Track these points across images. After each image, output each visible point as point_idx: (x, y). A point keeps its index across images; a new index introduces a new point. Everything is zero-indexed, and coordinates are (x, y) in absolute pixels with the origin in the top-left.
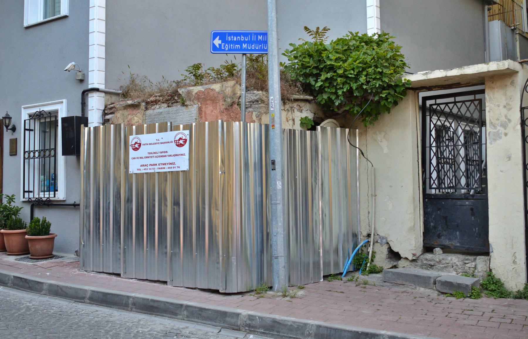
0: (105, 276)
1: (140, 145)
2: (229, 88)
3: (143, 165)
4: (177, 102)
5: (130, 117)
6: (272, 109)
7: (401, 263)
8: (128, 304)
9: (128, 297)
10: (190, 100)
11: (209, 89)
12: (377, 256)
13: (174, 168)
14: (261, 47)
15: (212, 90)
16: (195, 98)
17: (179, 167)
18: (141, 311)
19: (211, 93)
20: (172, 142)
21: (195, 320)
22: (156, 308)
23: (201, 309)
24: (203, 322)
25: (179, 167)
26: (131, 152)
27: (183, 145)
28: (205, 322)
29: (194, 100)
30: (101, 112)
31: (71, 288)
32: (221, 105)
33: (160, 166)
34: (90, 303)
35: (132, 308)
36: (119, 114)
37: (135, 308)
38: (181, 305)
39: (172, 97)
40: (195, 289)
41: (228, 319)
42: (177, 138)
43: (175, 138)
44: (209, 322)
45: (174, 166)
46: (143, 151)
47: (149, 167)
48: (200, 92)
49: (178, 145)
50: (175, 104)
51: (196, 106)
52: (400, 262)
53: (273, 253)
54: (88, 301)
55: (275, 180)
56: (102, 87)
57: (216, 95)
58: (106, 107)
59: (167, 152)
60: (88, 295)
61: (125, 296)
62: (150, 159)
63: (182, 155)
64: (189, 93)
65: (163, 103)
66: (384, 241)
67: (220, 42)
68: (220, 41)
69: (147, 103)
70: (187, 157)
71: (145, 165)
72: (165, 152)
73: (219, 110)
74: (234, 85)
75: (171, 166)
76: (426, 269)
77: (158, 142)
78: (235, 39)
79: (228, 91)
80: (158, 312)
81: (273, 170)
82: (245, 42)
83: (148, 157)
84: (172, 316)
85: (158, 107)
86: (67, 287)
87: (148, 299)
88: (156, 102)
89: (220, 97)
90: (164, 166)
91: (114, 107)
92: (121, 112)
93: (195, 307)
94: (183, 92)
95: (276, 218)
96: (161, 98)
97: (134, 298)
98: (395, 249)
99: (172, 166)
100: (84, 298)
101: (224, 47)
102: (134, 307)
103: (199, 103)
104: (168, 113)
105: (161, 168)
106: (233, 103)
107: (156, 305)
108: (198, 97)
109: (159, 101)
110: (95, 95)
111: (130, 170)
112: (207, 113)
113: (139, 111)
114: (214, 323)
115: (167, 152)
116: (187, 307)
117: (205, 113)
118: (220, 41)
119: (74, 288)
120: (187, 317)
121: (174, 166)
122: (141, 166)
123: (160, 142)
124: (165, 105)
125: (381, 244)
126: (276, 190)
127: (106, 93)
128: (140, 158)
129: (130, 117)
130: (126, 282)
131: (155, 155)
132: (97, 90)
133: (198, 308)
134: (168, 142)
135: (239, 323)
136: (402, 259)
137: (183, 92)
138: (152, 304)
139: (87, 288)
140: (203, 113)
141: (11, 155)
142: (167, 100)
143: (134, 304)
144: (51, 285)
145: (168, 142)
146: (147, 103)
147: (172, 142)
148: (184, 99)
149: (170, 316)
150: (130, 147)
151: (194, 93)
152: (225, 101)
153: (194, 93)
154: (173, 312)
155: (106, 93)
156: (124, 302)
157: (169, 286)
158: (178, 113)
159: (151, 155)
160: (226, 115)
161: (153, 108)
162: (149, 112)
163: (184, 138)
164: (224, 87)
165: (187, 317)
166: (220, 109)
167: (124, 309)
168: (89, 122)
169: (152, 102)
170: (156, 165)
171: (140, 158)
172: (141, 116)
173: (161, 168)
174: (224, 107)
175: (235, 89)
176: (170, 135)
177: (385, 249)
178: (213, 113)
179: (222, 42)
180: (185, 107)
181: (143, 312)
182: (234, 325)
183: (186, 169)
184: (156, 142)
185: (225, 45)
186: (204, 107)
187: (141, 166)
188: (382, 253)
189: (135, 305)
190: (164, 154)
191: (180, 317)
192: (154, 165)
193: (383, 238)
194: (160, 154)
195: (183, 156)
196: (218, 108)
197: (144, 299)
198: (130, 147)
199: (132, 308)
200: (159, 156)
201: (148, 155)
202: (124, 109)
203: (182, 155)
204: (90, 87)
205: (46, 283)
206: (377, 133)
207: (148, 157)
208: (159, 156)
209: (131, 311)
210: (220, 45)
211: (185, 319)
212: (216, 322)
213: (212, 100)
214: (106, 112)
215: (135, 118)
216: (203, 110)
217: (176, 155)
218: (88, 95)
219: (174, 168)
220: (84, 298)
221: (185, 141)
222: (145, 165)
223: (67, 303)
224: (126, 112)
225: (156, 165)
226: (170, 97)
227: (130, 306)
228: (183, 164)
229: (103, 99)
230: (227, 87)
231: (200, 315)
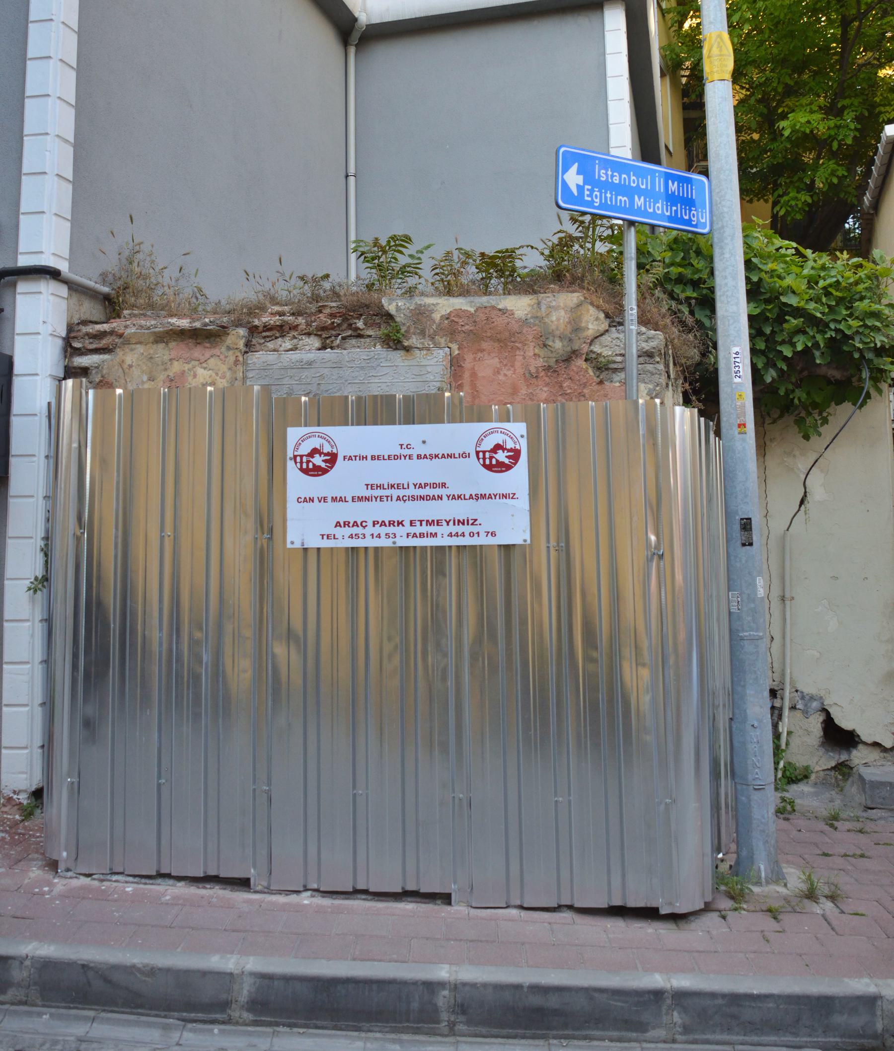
0: (181, 889)
1: (332, 459)
2: (562, 313)
3: (347, 524)
4: (360, 336)
5: (176, 367)
6: (737, 380)
7: (858, 756)
8: (436, 1010)
9: (431, 987)
10: (423, 333)
11: (493, 307)
12: (795, 742)
13: (472, 534)
14: (676, 211)
15: (503, 311)
16: (440, 328)
17: (493, 534)
18: (495, 1031)
19: (500, 321)
20: (465, 455)
21: (719, 1037)
22: (556, 1012)
23: (736, 999)
24: (747, 1038)
25: (493, 534)
26: (295, 478)
27: (508, 468)
28: (755, 1039)
29: (435, 333)
30: (59, 343)
31: (153, 972)
32: (532, 357)
33: (418, 529)
34: (256, 1023)
35: (452, 1025)
36: (130, 357)
37: (469, 1023)
38: (657, 994)
39: (345, 320)
40: (558, 909)
41: (839, 1019)
42: (487, 445)
43: (479, 443)
44: (773, 1038)
45: (474, 529)
46: (344, 479)
47: (370, 530)
48: (459, 313)
49: (489, 467)
50: (353, 341)
51: (441, 354)
52: (855, 752)
53: (750, 777)
54: (247, 1016)
55: (749, 573)
56: (63, 267)
57: (515, 327)
58: (70, 328)
59: (444, 485)
60: (245, 991)
61: (415, 983)
62: (373, 504)
63: (504, 496)
64: (421, 314)
65: (309, 334)
66: (815, 705)
67: (580, 180)
68: (581, 177)
69: (253, 330)
70: (523, 503)
71: (355, 524)
72: (434, 486)
73: (520, 371)
74: (579, 305)
75: (460, 529)
76: (78, 671)
77: (406, 452)
78: (616, 180)
79: (558, 319)
80: (565, 1026)
81: (744, 545)
82: (639, 191)
83: (367, 499)
84: (624, 1034)
85: (287, 344)
86: (130, 970)
87: (518, 987)
88: (282, 330)
89: (529, 333)
90: (433, 529)
91: (112, 333)
92: (140, 349)
93: (713, 995)
94: (398, 309)
95: (756, 679)
96: (301, 320)
97: (456, 987)
98: (845, 722)
99: (467, 529)
100: (224, 1006)
101: (590, 195)
102: (462, 1018)
103: (455, 346)
104: (337, 365)
105: (422, 535)
106: (569, 358)
107: (553, 1002)
108: (451, 327)
109: (295, 327)
110: (47, 289)
111: (289, 539)
112: (480, 375)
113: (216, 351)
114: (789, 1039)
115: (444, 485)
116: (681, 997)
117: (474, 375)
118: (581, 177)
119: (168, 971)
120: (686, 1030)
121: (474, 529)
122: (338, 524)
123: (415, 453)
124: (316, 342)
125: (806, 713)
126: (754, 601)
127: (74, 287)
128: (334, 499)
129: (176, 367)
130: (284, 908)
131: (395, 493)
132: (53, 274)
133: (724, 996)
134: (450, 456)
135: (879, 1026)
136: (860, 746)
137: (398, 309)
138: (536, 1000)
139: (229, 963)
140: (467, 375)
141: (750, 519)
142: (324, 329)
143: (461, 1009)
144: (47, 965)
145: (450, 456)
146: (253, 330)
147: (465, 455)
148: (403, 329)
149: (615, 1034)
150: (290, 464)
151: (437, 316)
152: (545, 345)
153: (437, 316)
154: (626, 1022)
155: (74, 287)
156: (415, 1005)
157: (458, 909)
158: (373, 368)
159: (376, 492)
160: (547, 385)
161: (271, 345)
162: (259, 358)
163: (510, 445)
164: (543, 307)
165: (686, 1030)
166: (527, 367)
167: (417, 1031)
168: (18, 368)
169: (267, 328)
170: (400, 523)
171: (334, 499)
172: (224, 368)
173: (422, 535)
174: (540, 362)
175: (580, 318)
176: (464, 435)
177: (815, 724)
178: (501, 377)
179: (585, 183)
180: (402, 353)
181: (504, 1032)
182: (863, 1036)
183: (519, 541)
184: (398, 451)
185: (592, 191)
186: (469, 357)
187: (338, 524)
188: (808, 733)
189: (464, 1012)
190: (431, 491)
191: (661, 1033)
192: (392, 523)
193: (812, 698)
194: (412, 491)
195: (508, 501)
196: (518, 364)
197: (499, 988)
198: (290, 464)
199: (452, 1025)
200: (413, 498)
201: (368, 493)
202: (156, 342)
203: (504, 496)
204: (23, 261)
205: (21, 960)
206: (797, 453)
207: (367, 499)
208: (413, 498)
209: (452, 1031)
210: (580, 188)
211: (678, 1037)
212: (796, 1035)
213: (499, 341)
214: (76, 345)
215: (200, 371)
216: (468, 364)
217: (483, 497)
218: (14, 285)
219: (472, 534)
220: (224, 1006)
221: (515, 455)
222: (355, 524)
223: (155, 1034)
224: (161, 352)
225: (400, 523)
226: (337, 321)
227: (444, 1016)
228: (509, 522)
229: (64, 305)
230: (557, 308)
231: (734, 1017)
